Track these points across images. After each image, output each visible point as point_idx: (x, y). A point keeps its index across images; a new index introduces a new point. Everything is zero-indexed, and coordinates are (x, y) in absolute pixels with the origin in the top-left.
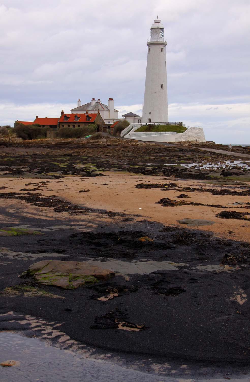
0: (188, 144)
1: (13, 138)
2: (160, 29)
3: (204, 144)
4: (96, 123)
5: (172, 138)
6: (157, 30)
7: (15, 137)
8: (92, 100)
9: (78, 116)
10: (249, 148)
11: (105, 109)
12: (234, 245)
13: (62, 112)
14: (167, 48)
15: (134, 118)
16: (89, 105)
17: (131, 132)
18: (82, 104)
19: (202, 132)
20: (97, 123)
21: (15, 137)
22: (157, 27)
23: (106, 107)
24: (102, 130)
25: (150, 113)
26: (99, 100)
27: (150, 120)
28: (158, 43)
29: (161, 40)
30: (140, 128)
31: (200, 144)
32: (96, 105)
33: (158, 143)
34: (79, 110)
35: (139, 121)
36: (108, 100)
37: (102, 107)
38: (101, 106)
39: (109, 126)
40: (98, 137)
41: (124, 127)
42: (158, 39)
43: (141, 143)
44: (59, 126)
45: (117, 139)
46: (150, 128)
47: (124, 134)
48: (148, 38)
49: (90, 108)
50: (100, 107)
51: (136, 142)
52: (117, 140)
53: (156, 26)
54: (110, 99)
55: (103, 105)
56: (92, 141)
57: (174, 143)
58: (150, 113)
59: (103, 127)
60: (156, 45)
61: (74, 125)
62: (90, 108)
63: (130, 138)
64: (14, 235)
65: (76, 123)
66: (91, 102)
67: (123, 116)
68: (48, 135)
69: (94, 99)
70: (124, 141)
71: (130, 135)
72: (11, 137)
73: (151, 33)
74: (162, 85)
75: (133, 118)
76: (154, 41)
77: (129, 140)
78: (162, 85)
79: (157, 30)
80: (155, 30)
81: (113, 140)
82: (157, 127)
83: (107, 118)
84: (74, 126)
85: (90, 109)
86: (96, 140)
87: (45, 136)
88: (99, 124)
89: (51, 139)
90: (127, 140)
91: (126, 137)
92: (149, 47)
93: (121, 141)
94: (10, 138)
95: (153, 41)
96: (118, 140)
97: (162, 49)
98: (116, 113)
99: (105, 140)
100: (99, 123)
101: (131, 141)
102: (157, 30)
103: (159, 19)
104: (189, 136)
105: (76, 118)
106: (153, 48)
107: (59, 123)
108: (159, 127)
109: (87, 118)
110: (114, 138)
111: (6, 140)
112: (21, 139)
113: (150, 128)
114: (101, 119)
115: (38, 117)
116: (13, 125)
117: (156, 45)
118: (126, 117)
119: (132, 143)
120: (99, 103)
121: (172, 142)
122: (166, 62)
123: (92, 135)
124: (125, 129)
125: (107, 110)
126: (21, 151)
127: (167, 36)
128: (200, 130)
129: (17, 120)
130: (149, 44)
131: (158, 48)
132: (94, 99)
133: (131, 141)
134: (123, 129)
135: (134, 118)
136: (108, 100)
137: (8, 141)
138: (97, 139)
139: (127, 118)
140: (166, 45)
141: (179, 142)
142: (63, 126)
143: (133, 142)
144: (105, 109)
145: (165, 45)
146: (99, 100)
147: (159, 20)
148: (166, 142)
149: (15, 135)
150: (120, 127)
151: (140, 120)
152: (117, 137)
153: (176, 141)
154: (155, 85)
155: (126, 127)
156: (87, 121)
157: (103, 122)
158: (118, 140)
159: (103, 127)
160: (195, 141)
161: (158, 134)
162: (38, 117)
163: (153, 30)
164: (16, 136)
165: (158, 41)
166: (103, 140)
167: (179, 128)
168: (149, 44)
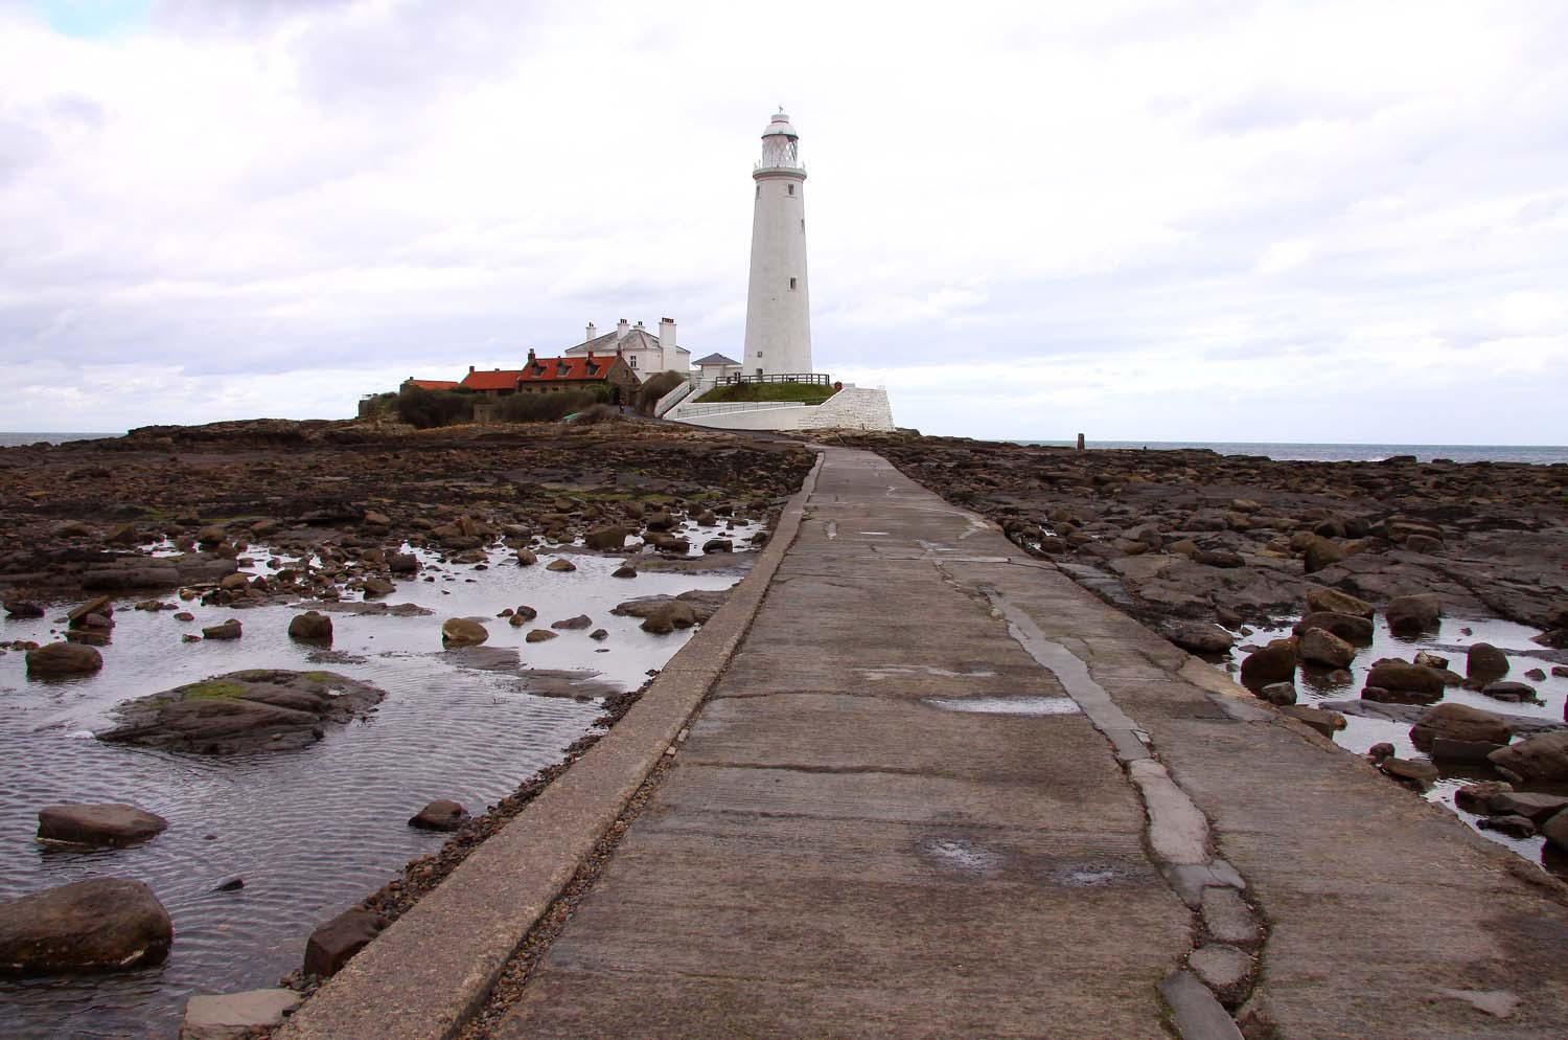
1: (388, 422)
2: (786, 139)
3: (879, 436)
4: (610, 380)
5: (789, 418)
6: (780, 139)
7: (395, 421)
9: (565, 364)
12: (1191, 715)
13: (531, 356)
14: (807, 187)
16: (612, 336)
18: (1182, 640)
21: (395, 421)
25: (760, 355)
26: (640, 323)
27: (760, 371)
29: (787, 164)
33: (756, 435)
41: (664, 387)
46: (738, 391)
48: (754, 155)
50: (639, 341)
53: (776, 129)
58: (760, 355)
60: (778, 178)
65: (559, 381)
68: (477, 416)
69: (623, 321)
72: (379, 422)
74: (793, 281)
78: (793, 281)
79: (779, 139)
80: (772, 140)
84: (544, 390)
87: (470, 417)
89: (481, 424)
97: (791, 188)
100: (621, 380)
102: (780, 139)
104: (839, 414)
105: (561, 370)
106: (766, 184)
107: (520, 382)
113: (738, 391)
115: (476, 370)
116: (397, 390)
117: (778, 178)
120: (639, 332)
127: (806, 156)
128: (877, 396)
130: (758, 176)
131: (780, 185)
132: (623, 321)
134: (661, 395)
141: (805, 431)
142: (530, 390)
145: (802, 177)
149: (393, 416)
154: (777, 273)
156: (589, 376)
162: (476, 370)
164: (396, 417)
167: (816, 392)
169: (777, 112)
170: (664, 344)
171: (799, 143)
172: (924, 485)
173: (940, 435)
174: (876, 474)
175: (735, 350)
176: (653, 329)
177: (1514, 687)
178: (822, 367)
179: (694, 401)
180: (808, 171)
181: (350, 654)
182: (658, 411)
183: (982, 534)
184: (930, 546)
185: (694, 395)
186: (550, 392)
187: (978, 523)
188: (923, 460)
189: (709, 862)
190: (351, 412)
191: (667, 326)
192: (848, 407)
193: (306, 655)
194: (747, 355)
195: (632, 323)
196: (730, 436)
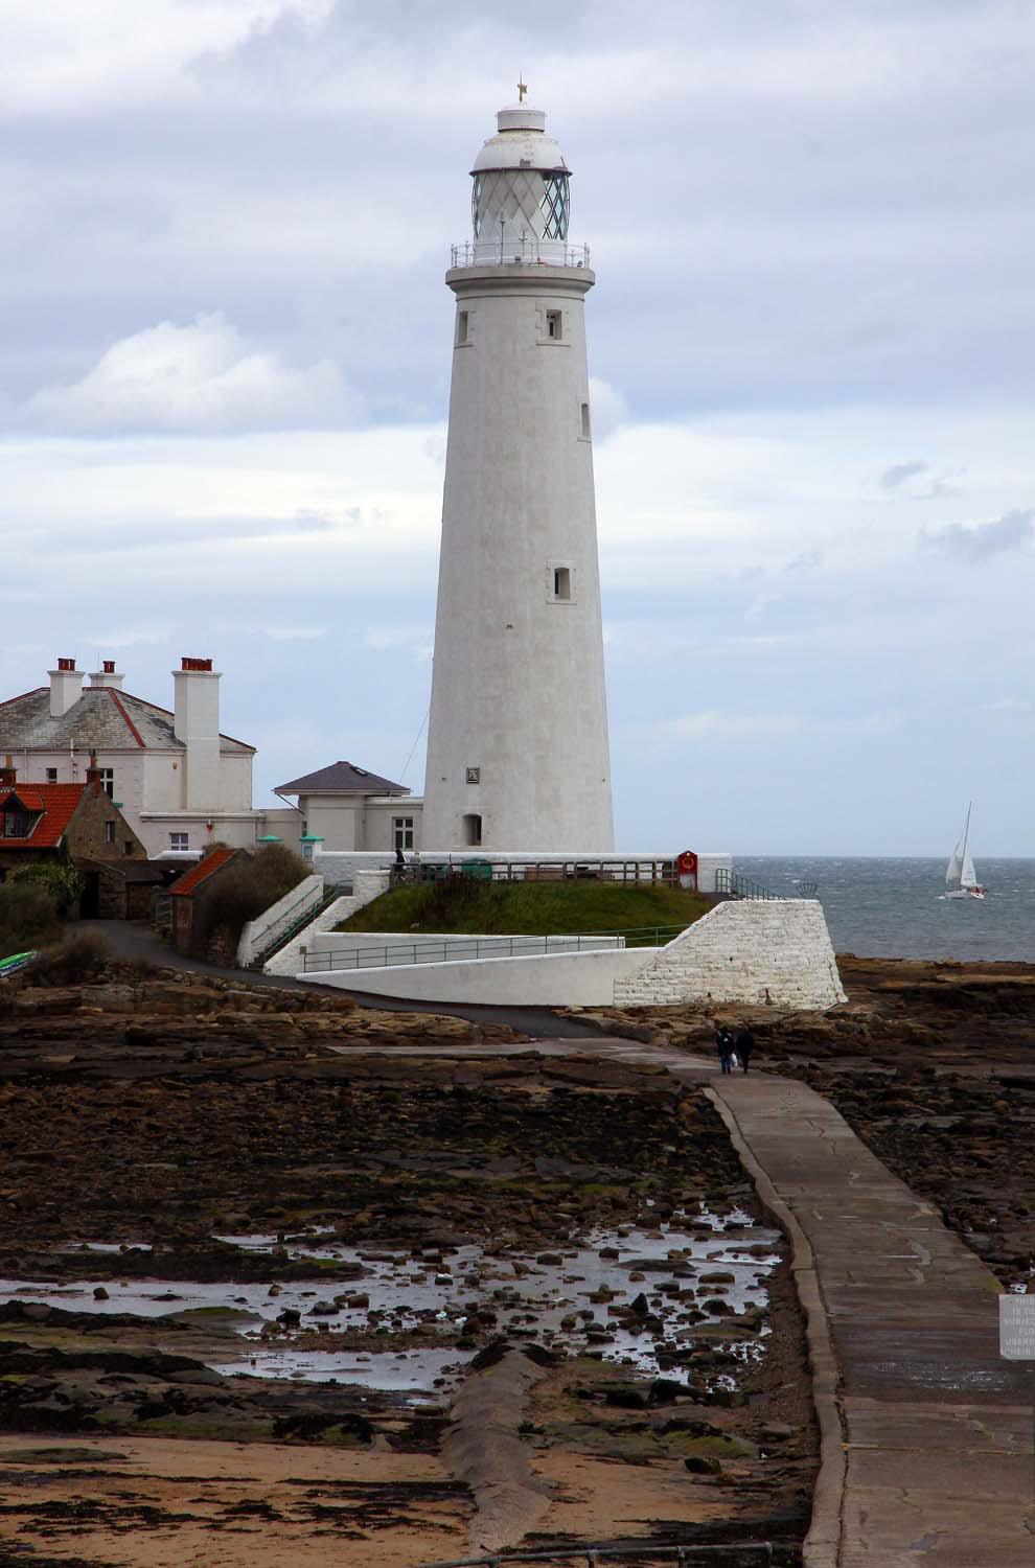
0: (690, 1028)
2: (539, 177)
4: (73, 852)
8: (52, 674)
11: (150, 737)
14: (590, 317)
15: (366, 808)
17: (316, 931)
20: (87, 855)
22: (517, 164)
23: (162, 722)
24: (122, 901)
25: (473, 777)
26: (109, 666)
28: (526, 273)
29: (554, 256)
30: (377, 900)
31: (779, 1025)
35: (404, 829)
36: (176, 674)
37: (129, 723)
38: (120, 720)
39: (170, 872)
40: (79, 967)
42: (528, 247)
43: (367, 1015)
45: (208, 984)
47: (261, 946)
48: (449, 229)
49: (42, 733)
50: (116, 723)
51: (339, 1009)
52: (212, 993)
53: (510, 154)
54: (190, 664)
55: (138, 703)
56: (31, 997)
57: (596, 1017)
58: (473, 777)
59: (128, 884)
62: (37, 732)
63: (300, 976)
64: (811, 1397)
66: (46, 682)
67: (279, 791)
69: (66, 665)
70: (255, 1001)
71: (303, 950)
73: (476, 200)
74: (561, 576)
75: (357, 804)
76: (495, 259)
77: (292, 996)
78: (561, 576)
81: (182, 995)
82: (495, 898)
83: (157, 803)
85: (42, 743)
86: (63, 994)
88: (94, 857)
90: (276, 994)
91: (274, 966)
92: (469, 305)
93: (239, 1004)
95: (495, 259)
96: (219, 988)
97: (554, 319)
98: (234, 764)
99: (125, 991)
100: (94, 849)
101: (305, 1004)
103: (531, 102)
106: (488, 309)
108: (508, 894)
109: (10, 818)
110: (187, 978)
114: (115, 824)
118: (303, 799)
119: (308, 1017)
120: (107, 701)
121: (586, 1009)
122: (585, 406)
123: (32, 954)
124: (273, 914)
125: (166, 743)
127: (595, 237)
130: (464, 284)
131: (527, 312)
132: (66, 665)
133: (305, 1004)
134: (256, 911)
135: (366, 808)
136: (176, 674)
138: (71, 980)
139: (311, 803)
140: (584, 285)
143: (315, 1006)
144: (150, 737)
146: (109, 666)
147: (529, 113)
148: (548, 1011)
150: (238, 885)
151: (409, 823)
152: (213, 964)
153: (619, 1004)
154: (508, 567)
155: (279, 898)
157: (132, 845)
158: (219, 988)
159: (128, 884)
160: (753, 1001)
161: (498, 949)
163: (482, 177)
165: (526, 259)
166: (110, 988)
168: (464, 284)
169: (510, 100)
170: (189, 732)
172: (893, 1169)
174: (828, 1148)
175: (399, 755)
176: (149, 681)
178: (633, 836)
179: (340, 926)
180: (569, 170)
181: (692, 1239)
182: (248, 951)
183: (927, 1217)
184: (886, 1224)
185: (339, 909)
187: (926, 1209)
188: (901, 1112)
191: (195, 680)
192: (730, 949)
193: (692, 1239)
194: (436, 775)
195: (89, 665)
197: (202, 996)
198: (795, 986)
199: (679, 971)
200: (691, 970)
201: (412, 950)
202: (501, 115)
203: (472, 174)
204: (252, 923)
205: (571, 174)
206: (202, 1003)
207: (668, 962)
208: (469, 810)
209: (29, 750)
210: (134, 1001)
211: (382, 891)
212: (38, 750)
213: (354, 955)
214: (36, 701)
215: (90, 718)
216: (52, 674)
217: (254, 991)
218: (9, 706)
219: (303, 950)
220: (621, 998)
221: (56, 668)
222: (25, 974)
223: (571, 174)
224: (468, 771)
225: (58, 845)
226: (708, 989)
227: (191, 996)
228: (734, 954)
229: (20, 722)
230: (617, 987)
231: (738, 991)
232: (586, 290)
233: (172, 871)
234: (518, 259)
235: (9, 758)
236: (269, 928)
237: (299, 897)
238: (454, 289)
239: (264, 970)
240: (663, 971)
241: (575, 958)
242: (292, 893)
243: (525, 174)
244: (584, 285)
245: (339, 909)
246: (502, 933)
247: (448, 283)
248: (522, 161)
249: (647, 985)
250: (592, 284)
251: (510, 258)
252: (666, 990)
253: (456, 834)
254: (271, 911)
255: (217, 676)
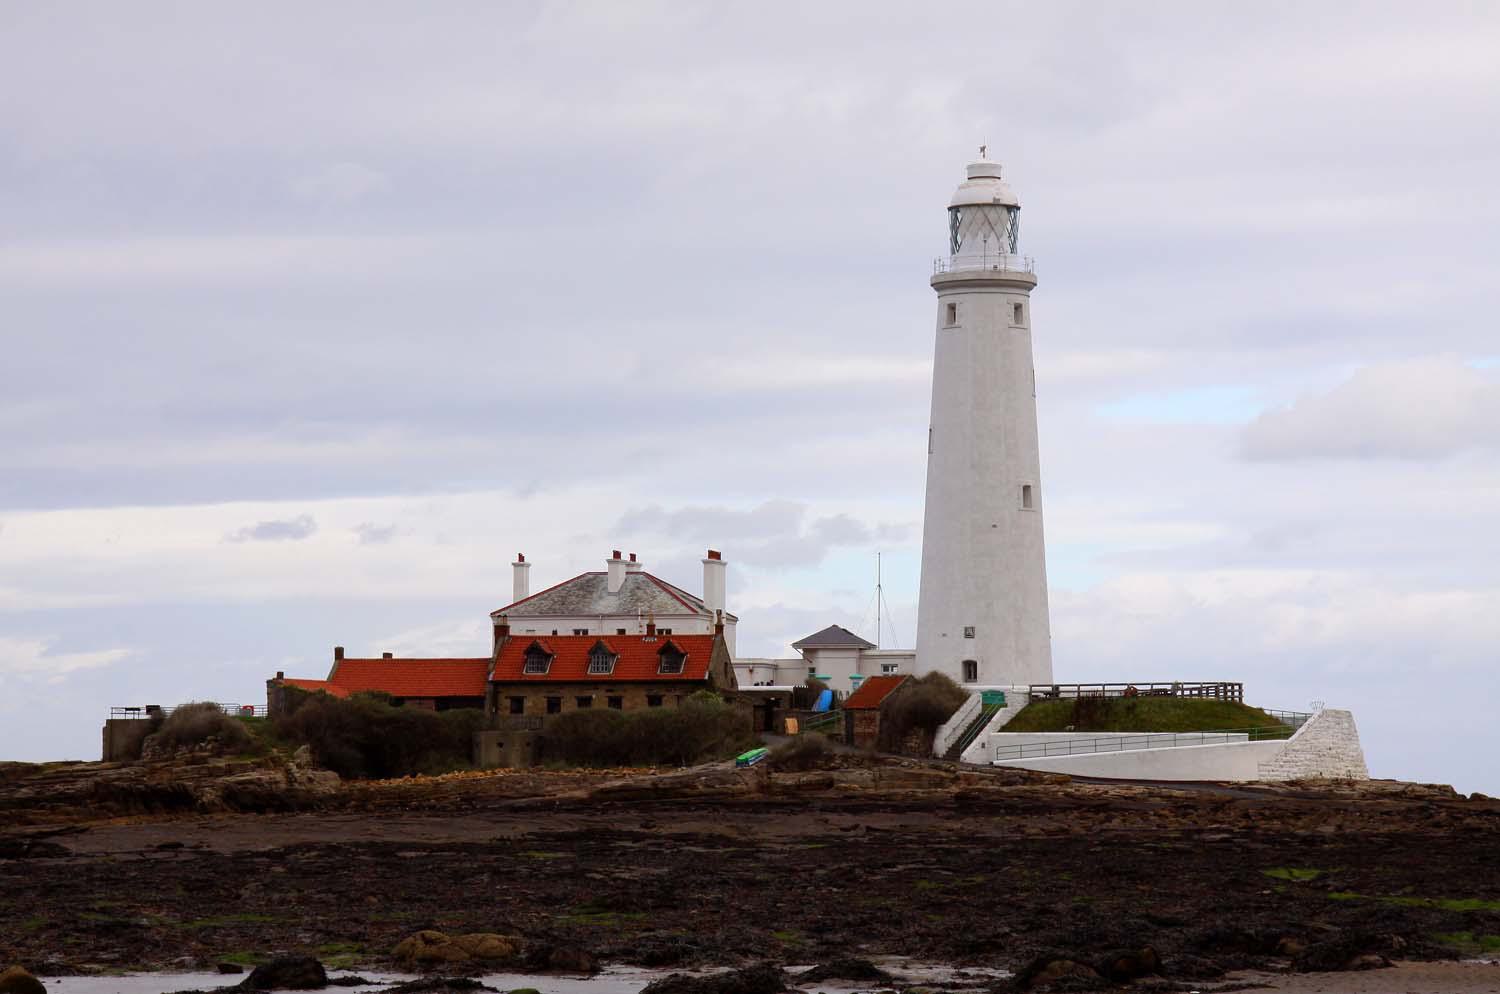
2: (1005, 212)
8: (609, 561)
10: (1496, 808)
16: (587, 585)
17: (989, 732)
19: (1351, 735)
22: (991, 201)
25: (969, 634)
28: (1003, 277)
29: (1015, 266)
32: (630, 585)
34: (543, 615)
36: (705, 562)
44: (495, 702)
48: (930, 244)
53: (984, 193)
58: (969, 634)
61: (586, 694)
65: (596, 684)
66: (604, 567)
67: (796, 645)
74: (1026, 489)
75: (855, 654)
76: (972, 264)
79: (992, 214)
84: (585, 702)
87: (467, 754)
91: (972, 754)
94: (288, 771)
97: (1018, 308)
99: (867, 774)
102: (982, 215)
106: (967, 302)
107: (496, 684)
111: (277, 783)
112: (330, 774)
121: (1250, 783)
126: (343, 831)
127: (1034, 246)
129: (280, 675)
130: (941, 285)
131: (1002, 301)
132: (617, 555)
134: (944, 718)
135: (861, 658)
136: (705, 562)
137: (283, 786)
139: (821, 654)
145: (1026, 285)
156: (661, 674)
162: (347, 656)
171: (1022, 216)
173: (38, 758)
177: (1391, 789)
179: (1003, 729)
186: (669, 705)
189: (1282, 969)
190: (91, 751)
196: (1139, 789)
197: (936, 776)
198: (1284, 769)
199: (1302, 757)
200: (1308, 757)
201: (1068, 745)
202: (970, 168)
203: (950, 209)
204: (945, 726)
205: (1019, 208)
206: (938, 780)
207: (1294, 750)
208: (968, 657)
209: (604, 616)
210: (874, 780)
211: (1025, 704)
212: (610, 616)
213: (1043, 747)
214: (588, 581)
215: (640, 593)
216: (609, 561)
217: (980, 772)
218: (569, 585)
219: (983, 745)
220: (1263, 776)
221: (611, 557)
222: (769, 764)
223: (1019, 208)
224: (966, 629)
225: (706, 677)
226: (1320, 769)
227: (929, 776)
228: (1331, 745)
229: (584, 597)
230: (1261, 767)
231: (1337, 771)
232: (1030, 289)
233: (773, 699)
234: (995, 267)
235: (651, 620)
236: (954, 729)
237: (970, 708)
238: (937, 289)
239: (961, 759)
240: (1291, 756)
241: (1228, 747)
242: (965, 705)
243: (998, 208)
244: (1029, 285)
245: (1001, 717)
246: (1149, 731)
247: (932, 285)
248: (995, 199)
249: (1282, 766)
250: (1036, 285)
251: (990, 267)
252: (1295, 770)
253: (679, 697)
254: (954, 717)
255: (725, 564)
